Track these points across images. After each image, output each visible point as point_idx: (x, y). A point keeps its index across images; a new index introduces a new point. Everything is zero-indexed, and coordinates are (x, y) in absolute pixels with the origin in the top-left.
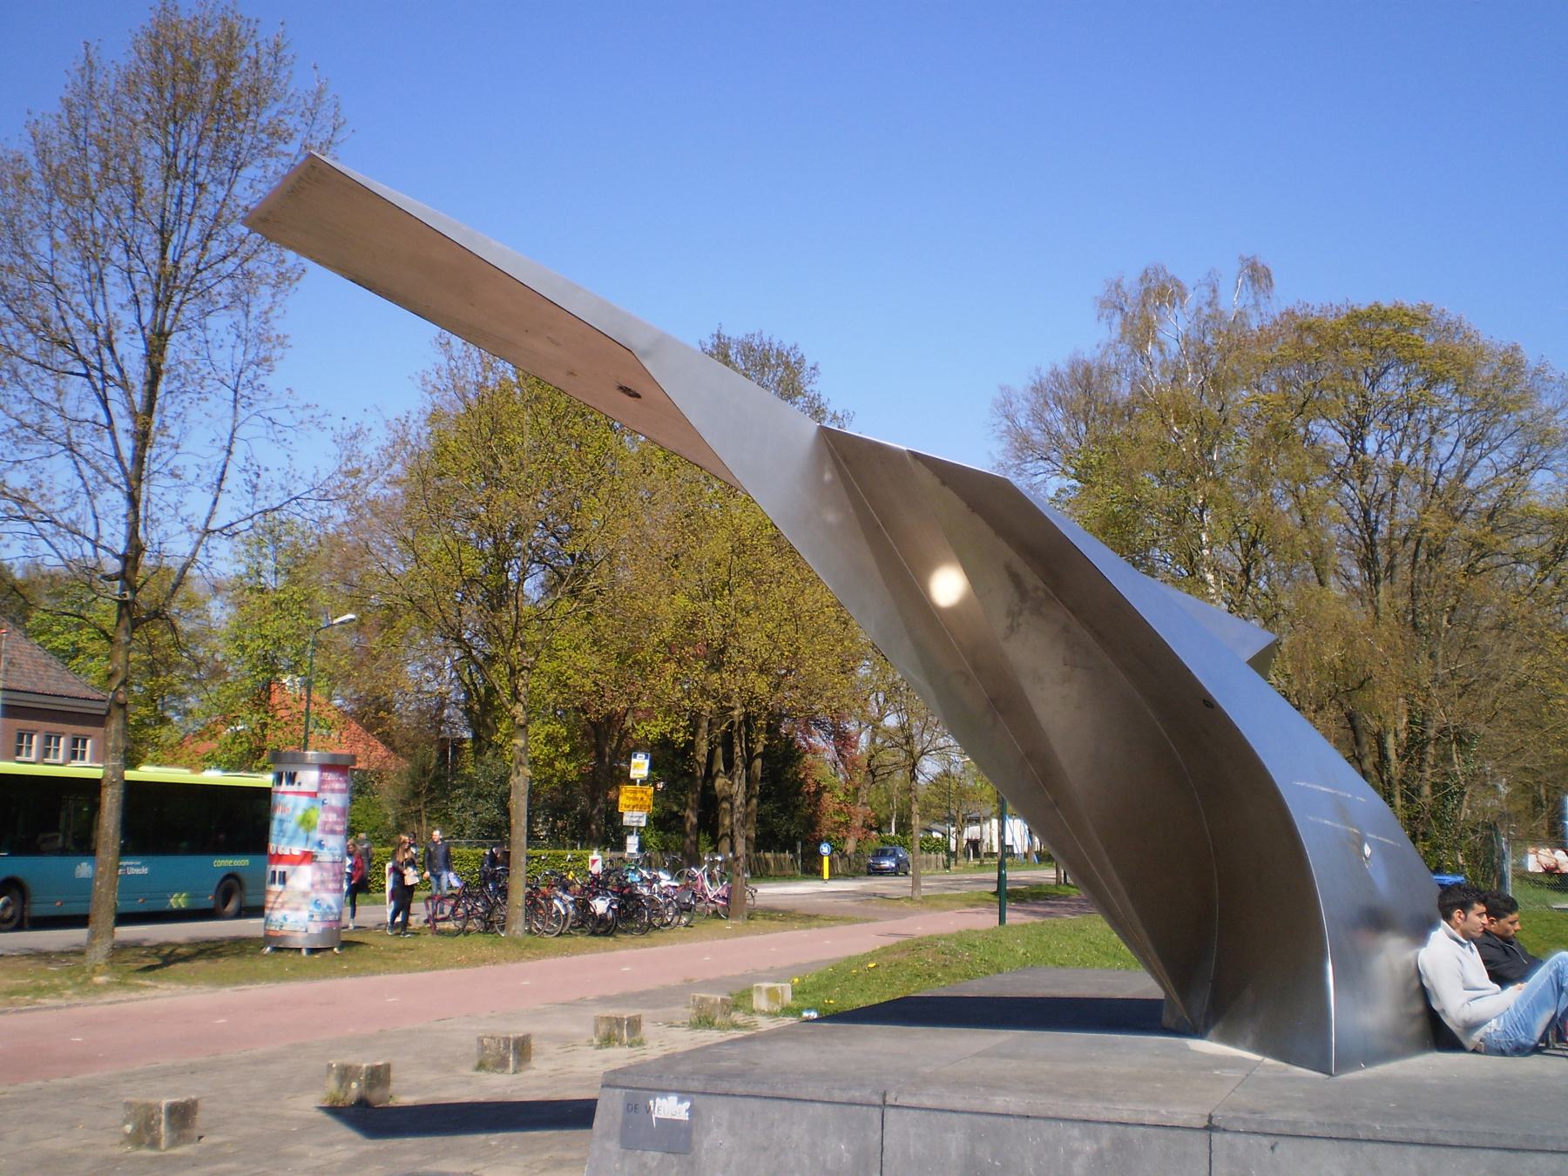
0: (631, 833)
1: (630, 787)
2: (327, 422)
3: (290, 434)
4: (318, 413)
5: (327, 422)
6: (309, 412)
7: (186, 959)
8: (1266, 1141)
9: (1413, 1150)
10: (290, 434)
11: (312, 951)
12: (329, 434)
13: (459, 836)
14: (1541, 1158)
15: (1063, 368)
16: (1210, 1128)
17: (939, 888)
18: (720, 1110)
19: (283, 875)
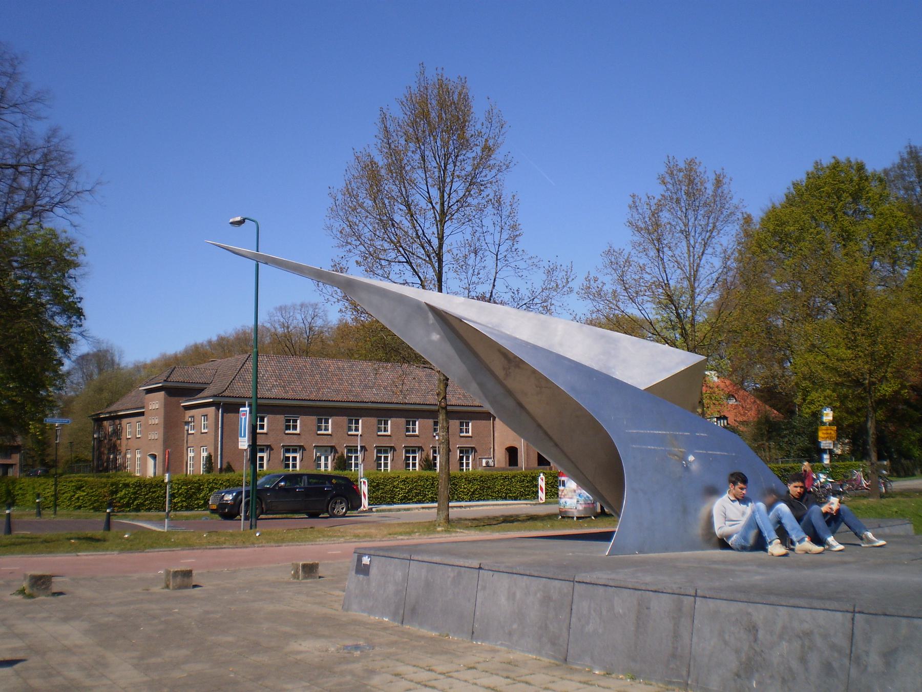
0: (826, 453)
1: (824, 427)
2: (541, 264)
3: (525, 273)
4: (535, 261)
5: (541, 264)
6: (533, 260)
7: (523, 521)
8: (491, 573)
9: (525, 577)
10: (525, 273)
11: (578, 518)
12: (542, 270)
13: (788, 457)
14: (557, 582)
15: (214, 338)
16: (480, 568)
17: (315, 483)
18: (377, 560)
19: (564, 482)
